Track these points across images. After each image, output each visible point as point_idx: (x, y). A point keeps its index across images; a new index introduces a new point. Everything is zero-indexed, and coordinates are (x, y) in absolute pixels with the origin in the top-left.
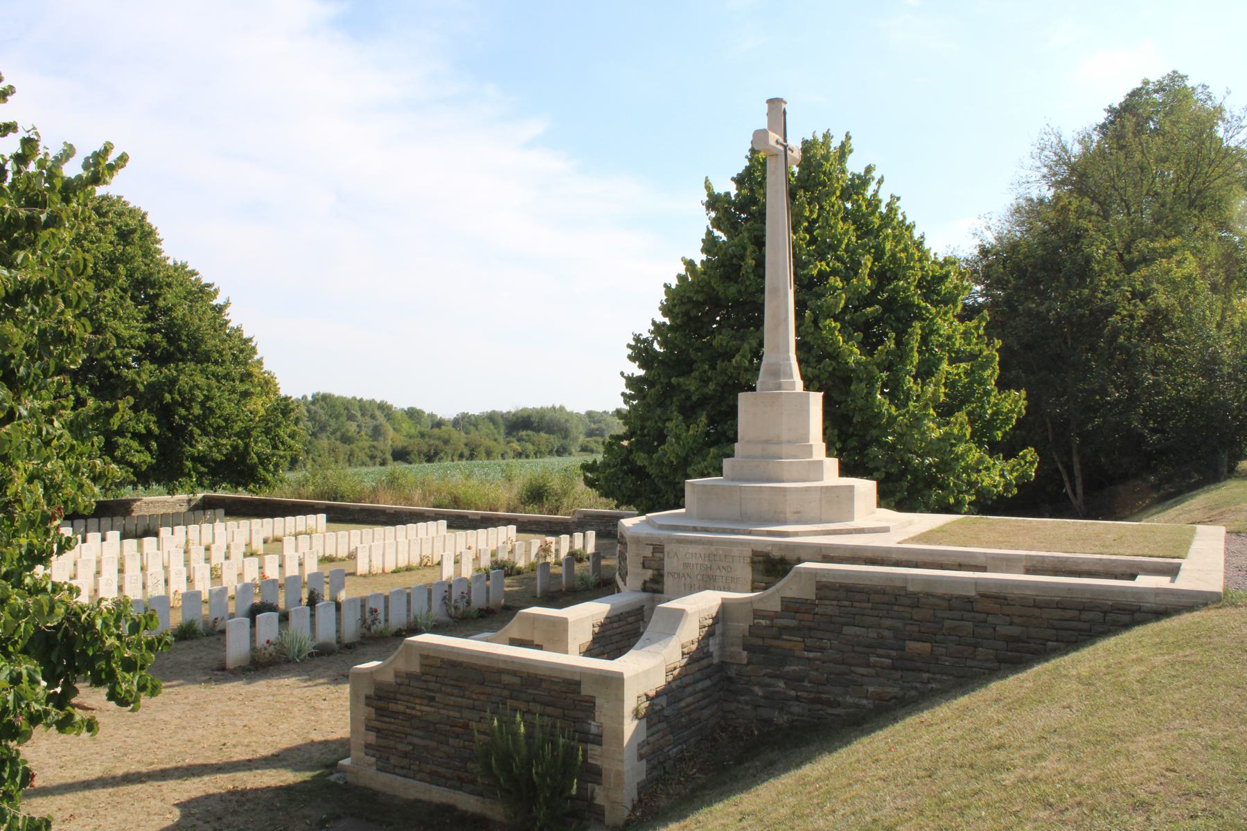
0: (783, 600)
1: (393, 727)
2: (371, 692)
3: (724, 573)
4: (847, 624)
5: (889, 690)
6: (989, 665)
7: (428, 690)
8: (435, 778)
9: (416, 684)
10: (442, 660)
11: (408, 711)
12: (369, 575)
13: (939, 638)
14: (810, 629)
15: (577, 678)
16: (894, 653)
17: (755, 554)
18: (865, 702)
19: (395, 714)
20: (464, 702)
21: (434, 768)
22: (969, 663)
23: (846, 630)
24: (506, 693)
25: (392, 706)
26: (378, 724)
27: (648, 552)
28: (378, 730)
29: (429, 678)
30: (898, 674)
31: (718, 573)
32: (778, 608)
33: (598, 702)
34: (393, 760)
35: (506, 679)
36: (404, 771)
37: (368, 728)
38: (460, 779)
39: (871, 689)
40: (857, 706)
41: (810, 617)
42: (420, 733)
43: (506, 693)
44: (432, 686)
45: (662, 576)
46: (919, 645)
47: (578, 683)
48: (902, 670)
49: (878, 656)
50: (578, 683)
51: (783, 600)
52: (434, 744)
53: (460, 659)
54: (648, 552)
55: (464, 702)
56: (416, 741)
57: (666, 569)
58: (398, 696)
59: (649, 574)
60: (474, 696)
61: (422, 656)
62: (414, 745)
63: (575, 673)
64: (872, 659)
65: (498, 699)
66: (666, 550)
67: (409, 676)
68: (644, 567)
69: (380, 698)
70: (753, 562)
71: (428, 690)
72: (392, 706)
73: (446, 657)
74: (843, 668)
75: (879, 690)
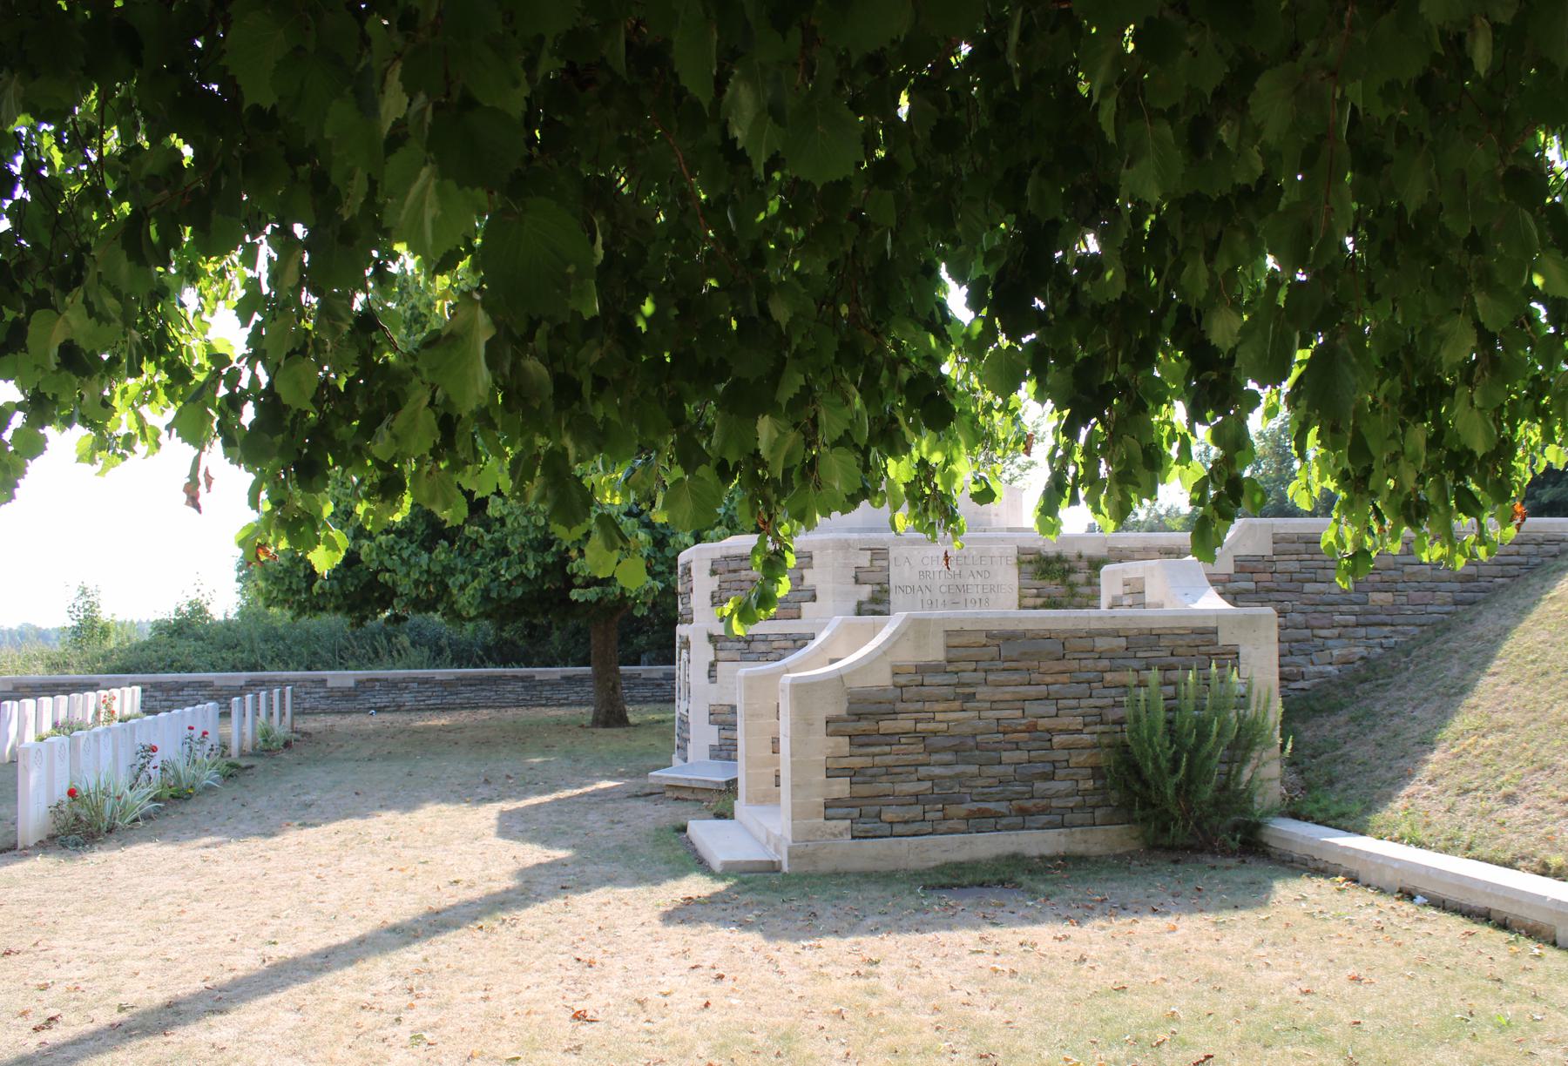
0: (1237, 559)
1: (889, 760)
2: (841, 710)
3: (979, 580)
4: (1309, 581)
5: (1355, 650)
6: (1447, 609)
7: (960, 685)
8: (980, 820)
9: (939, 679)
10: (989, 635)
11: (920, 726)
12: (131, 685)
13: (1400, 586)
14: (1269, 590)
15: (1212, 624)
16: (1357, 608)
17: (1022, 551)
18: (1330, 668)
19: (891, 738)
20: (1032, 691)
21: (975, 806)
22: (1430, 609)
23: (1308, 587)
24: (1105, 663)
25: (886, 726)
26: (857, 762)
27: (864, 560)
28: (853, 774)
29: (962, 665)
30: (1362, 632)
31: (971, 581)
32: (1231, 570)
33: (1243, 652)
34: (888, 815)
35: (1102, 644)
36: (915, 827)
37: (831, 773)
38: (1023, 812)
39: (1336, 652)
40: (1321, 675)
41: (1267, 576)
42: (948, 757)
43: (1105, 663)
44: (967, 677)
45: (887, 591)
46: (1383, 596)
47: (1215, 631)
48: (1365, 625)
49: (1341, 613)
50: (1215, 631)
51: (1237, 559)
52: (974, 769)
53: (1021, 627)
54: (864, 560)
55: (1032, 691)
56: (937, 771)
57: (894, 582)
58: (900, 706)
59: (865, 592)
60: (1048, 679)
61: (948, 633)
62: (931, 778)
63: (1208, 617)
64: (1337, 618)
65: (1091, 675)
66: (892, 555)
67: (921, 669)
68: (857, 581)
69: (859, 716)
70: (1020, 562)
71: (960, 685)
72: (886, 726)
73: (995, 627)
74: (1308, 632)
75: (1344, 651)
